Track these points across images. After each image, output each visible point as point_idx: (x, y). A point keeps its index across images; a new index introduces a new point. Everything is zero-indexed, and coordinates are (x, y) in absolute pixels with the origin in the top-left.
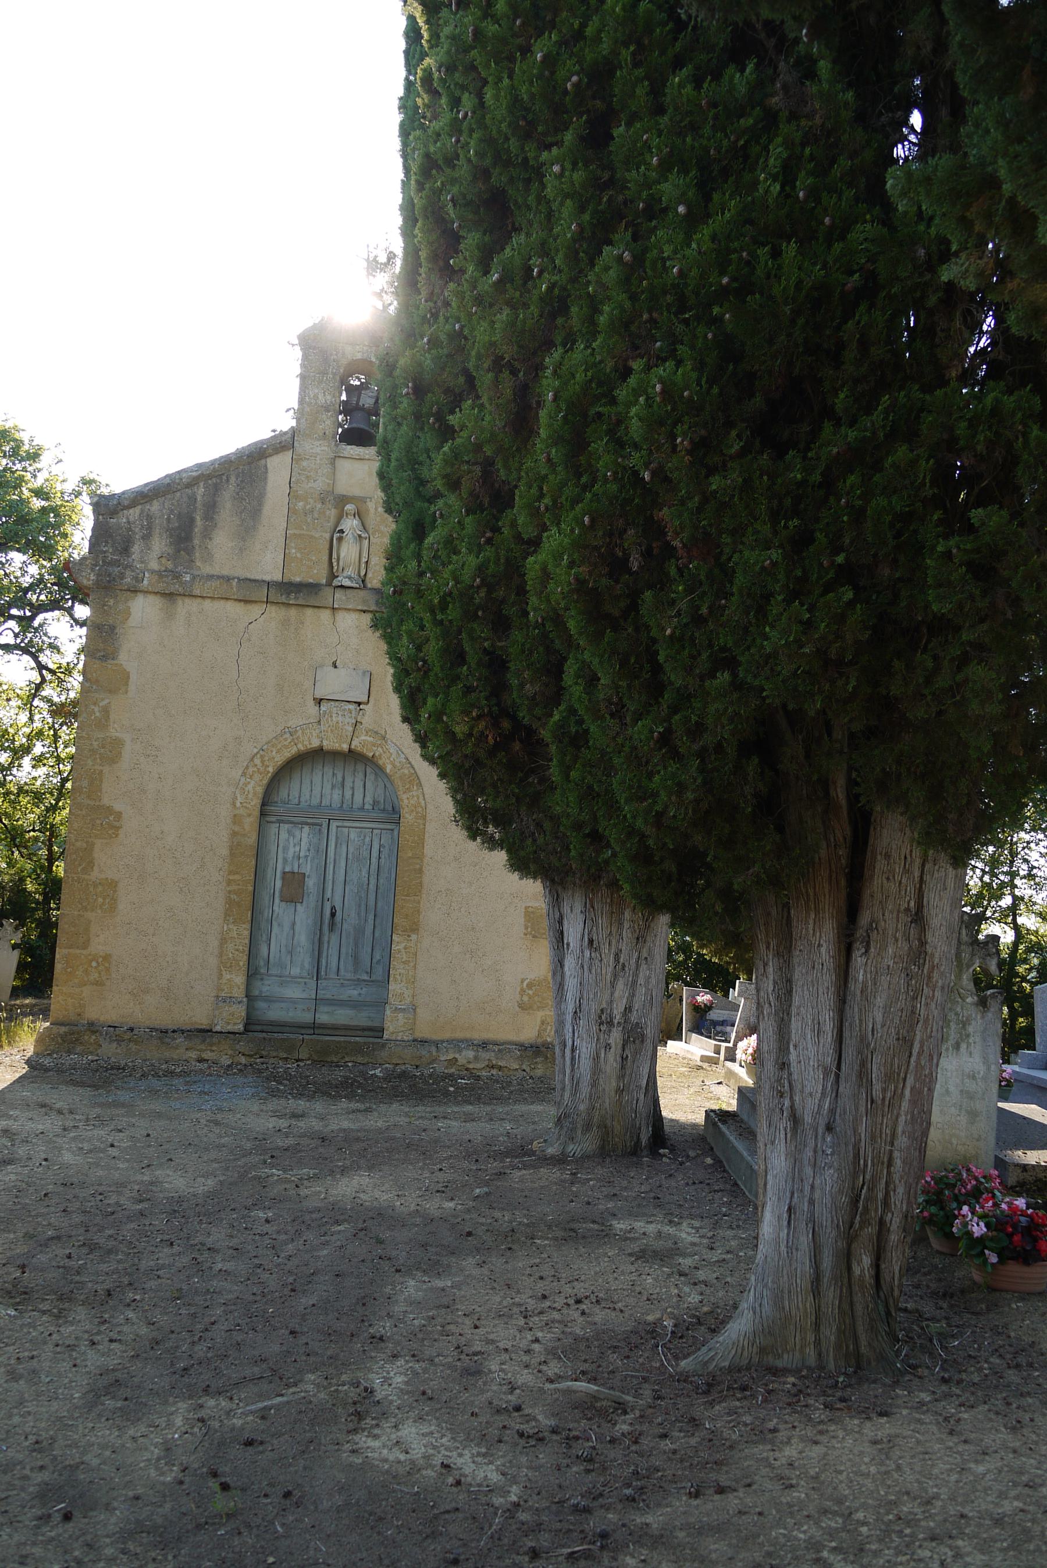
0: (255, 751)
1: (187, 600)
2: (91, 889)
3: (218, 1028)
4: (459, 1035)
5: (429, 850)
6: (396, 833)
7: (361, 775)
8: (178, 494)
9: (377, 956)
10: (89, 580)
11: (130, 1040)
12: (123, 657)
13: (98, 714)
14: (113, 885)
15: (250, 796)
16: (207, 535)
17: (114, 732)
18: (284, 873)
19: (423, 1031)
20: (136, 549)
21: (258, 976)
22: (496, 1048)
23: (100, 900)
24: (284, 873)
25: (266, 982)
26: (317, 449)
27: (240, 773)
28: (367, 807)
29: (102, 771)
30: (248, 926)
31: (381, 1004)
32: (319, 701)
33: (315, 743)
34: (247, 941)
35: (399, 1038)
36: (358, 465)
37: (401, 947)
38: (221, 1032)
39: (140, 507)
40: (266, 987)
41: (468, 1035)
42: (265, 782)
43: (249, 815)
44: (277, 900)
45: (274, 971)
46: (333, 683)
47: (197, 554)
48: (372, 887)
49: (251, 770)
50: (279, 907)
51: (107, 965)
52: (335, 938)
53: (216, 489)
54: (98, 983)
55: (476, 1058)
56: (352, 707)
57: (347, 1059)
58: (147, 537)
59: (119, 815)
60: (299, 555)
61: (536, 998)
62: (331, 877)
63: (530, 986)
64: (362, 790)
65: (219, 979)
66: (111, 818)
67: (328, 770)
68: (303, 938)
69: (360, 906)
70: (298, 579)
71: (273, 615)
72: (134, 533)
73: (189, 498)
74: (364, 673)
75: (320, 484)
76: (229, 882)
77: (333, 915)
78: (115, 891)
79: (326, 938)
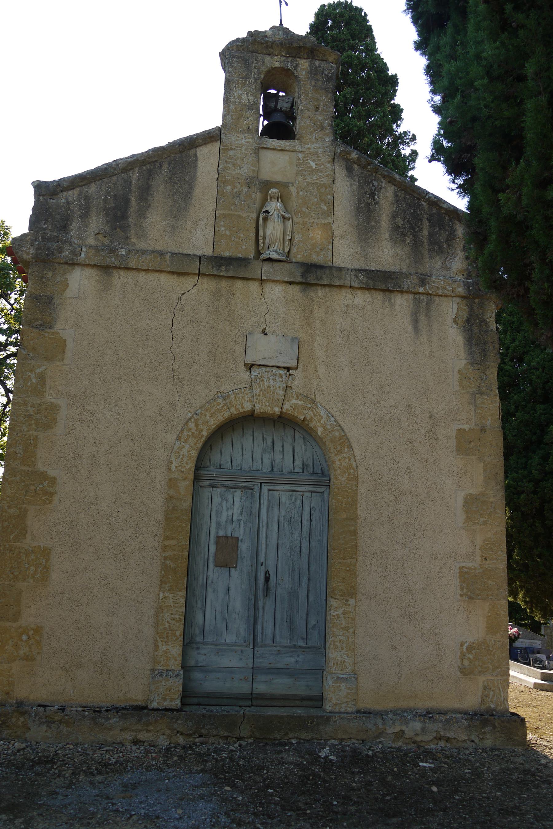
0: (190, 415)
1: (122, 273)
2: (23, 557)
3: (154, 705)
4: (403, 704)
5: (362, 512)
6: (326, 494)
7: (289, 440)
8: (115, 178)
9: (312, 622)
10: (28, 254)
11: (61, 722)
12: (60, 326)
13: (34, 381)
14: (46, 553)
15: (185, 460)
16: (142, 214)
17: (50, 398)
18: (218, 537)
19: (367, 702)
20: (74, 226)
21: (194, 645)
22: (443, 718)
23: (32, 569)
24: (218, 537)
25: (202, 651)
26: (242, 141)
27: (175, 437)
28: (296, 470)
29: (36, 437)
30: (183, 593)
31: (319, 672)
32: (250, 367)
33: (248, 407)
34: (183, 609)
35: (343, 710)
36: (279, 155)
37: (340, 612)
38: (158, 710)
39: (78, 189)
40: (202, 657)
41: (412, 704)
42: (199, 445)
43: (185, 479)
44: (211, 566)
45: (210, 639)
46: (264, 349)
47: (132, 231)
48: (305, 550)
49: (185, 434)
50: (213, 572)
51: (38, 638)
52: (269, 604)
53: (150, 174)
54: (28, 658)
55: (424, 730)
56: (282, 372)
57: (291, 735)
58: (85, 216)
59: (53, 481)
60: (228, 233)
61: (477, 663)
62: (264, 541)
63: (470, 649)
64: (291, 453)
65: (155, 650)
66: (45, 484)
67: (258, 435)
68: (238, 604)
69: (293, 570)
70: (227, 254)
71: (205, 286)
72: (73, 212)
73: (125, 181)
74: (293, 339)
75: (246, 170)
76: (165, 548)
77: (267, 579)
78: (48, 560)
79: (261, 604)
